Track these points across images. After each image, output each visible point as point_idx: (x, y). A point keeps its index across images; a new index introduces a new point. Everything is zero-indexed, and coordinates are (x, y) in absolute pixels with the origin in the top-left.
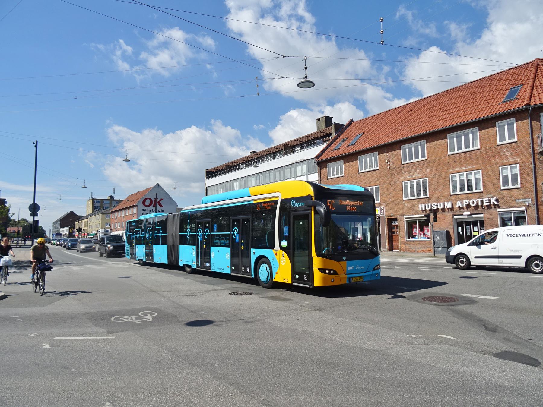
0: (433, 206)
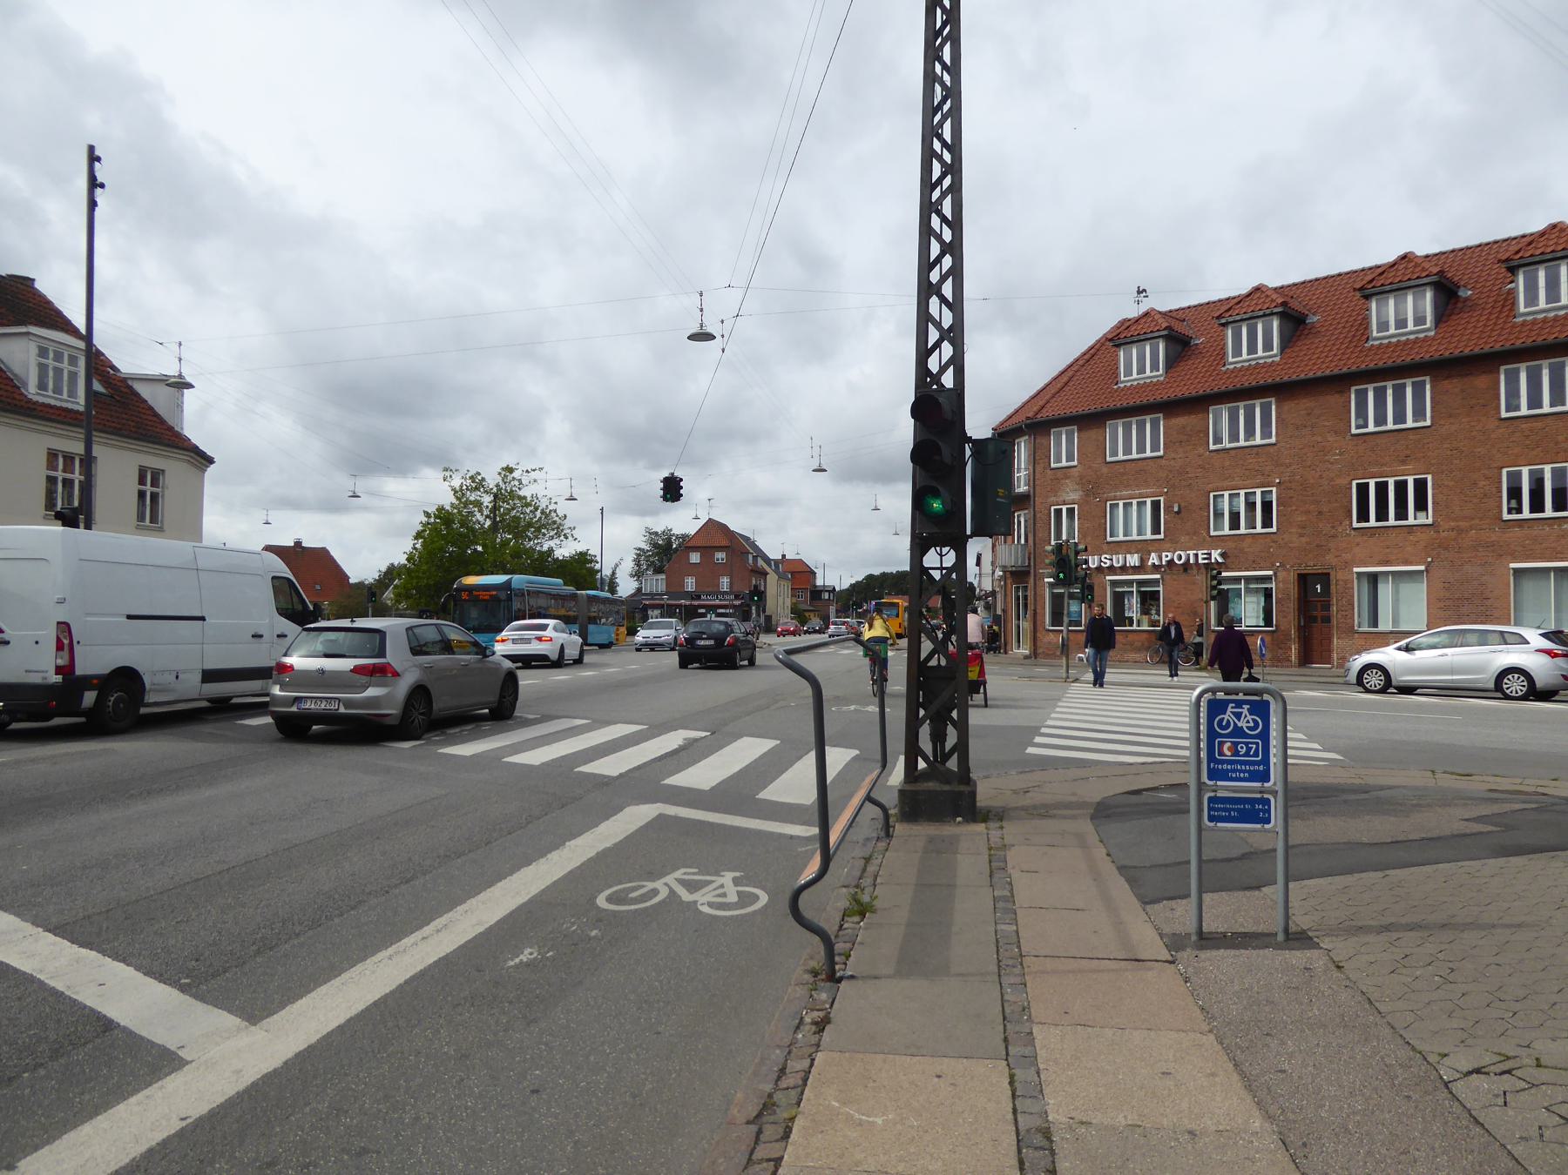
0: (1103, 560)
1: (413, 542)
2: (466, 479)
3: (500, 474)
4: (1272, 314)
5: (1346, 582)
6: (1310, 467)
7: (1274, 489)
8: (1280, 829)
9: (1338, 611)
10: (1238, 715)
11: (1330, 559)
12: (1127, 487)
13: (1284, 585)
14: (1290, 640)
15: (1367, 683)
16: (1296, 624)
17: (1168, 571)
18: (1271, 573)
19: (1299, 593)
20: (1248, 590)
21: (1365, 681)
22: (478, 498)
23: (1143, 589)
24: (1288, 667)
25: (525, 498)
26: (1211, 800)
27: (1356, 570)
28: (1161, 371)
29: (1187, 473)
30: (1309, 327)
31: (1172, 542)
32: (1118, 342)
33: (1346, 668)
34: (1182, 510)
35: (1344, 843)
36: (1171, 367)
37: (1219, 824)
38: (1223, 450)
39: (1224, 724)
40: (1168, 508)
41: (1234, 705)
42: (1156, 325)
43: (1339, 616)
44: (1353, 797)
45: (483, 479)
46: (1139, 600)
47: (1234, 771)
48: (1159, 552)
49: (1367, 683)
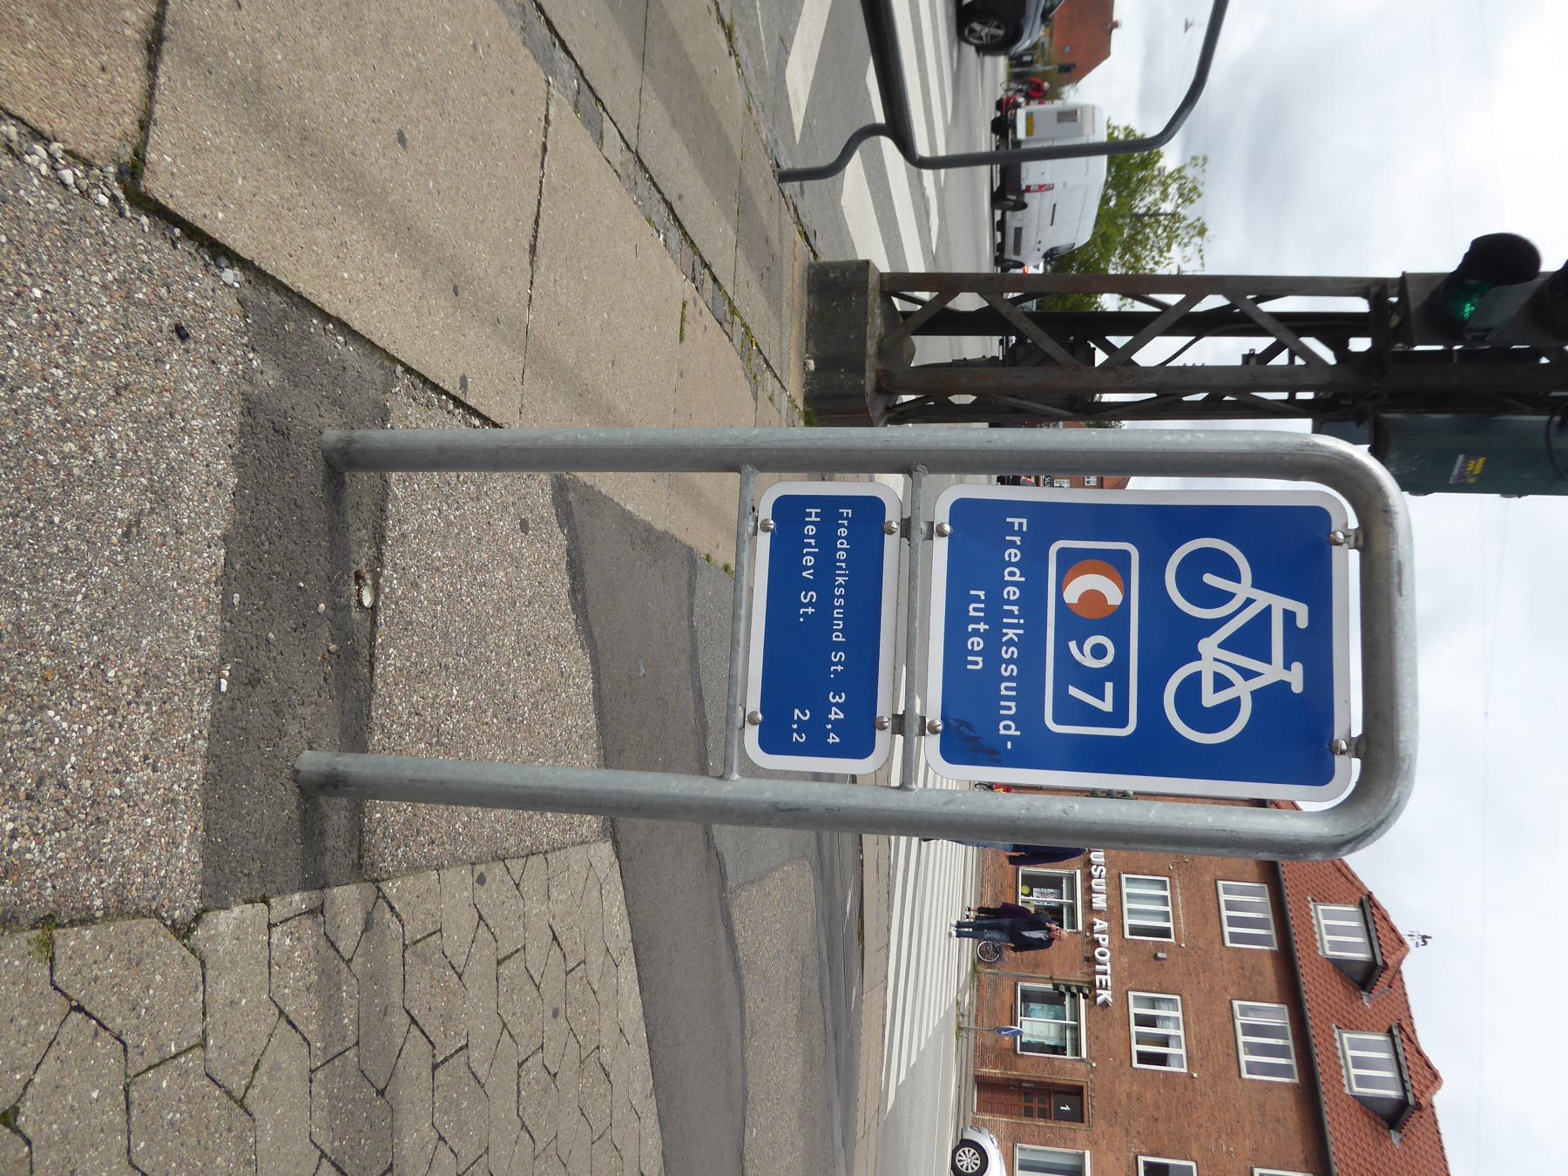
0: (1100, 868)
1: (1121, 128)
2: (1192, 182)
3: (1199, 219)
4: (1405, 1090)
5: (1074, 1140)
6: (1212, 1115)
7: (1184, 1070)
8: (736, 787)
9: (1039, 1126)
10: (1252, 640)
11: (1100, 1126)
12: (1187, 902)
13: (1068, 1069)
14: (1005, 1069)
15: (964, 1152)
16: (1024, 1078)
17: (1086, 940)
18: (1084, 1055)
19: (1061, 1085)
20: (1063, 1028)
21: (966, 1149)
22: (1170, 197)
23: (1065, 910)
24: (975, 1062)
25: (1169, 250)
26: (870, 509)
27: (1088, 1153)
28: (1329, 953)
29: (1204, 972)
30: (1386, 1132)
31: (1121, 947)
32: (1367, 906)
33: (982, 1128)
34: (1159, 963)
35: (745, 1090)
36: (1334, 965)
37: (764, 542)
38: (1233, 1016)
39: (1210, 579)
40: (1161, 947)
41: (1302, 622)
42: (1388, 951)
43: (1033, 1128)
44: (837, 1117)
45: (1192, 202)
46: (1053, 904)
47: (995, 612)
48: (1109, 932)
49: (964, 1152)
